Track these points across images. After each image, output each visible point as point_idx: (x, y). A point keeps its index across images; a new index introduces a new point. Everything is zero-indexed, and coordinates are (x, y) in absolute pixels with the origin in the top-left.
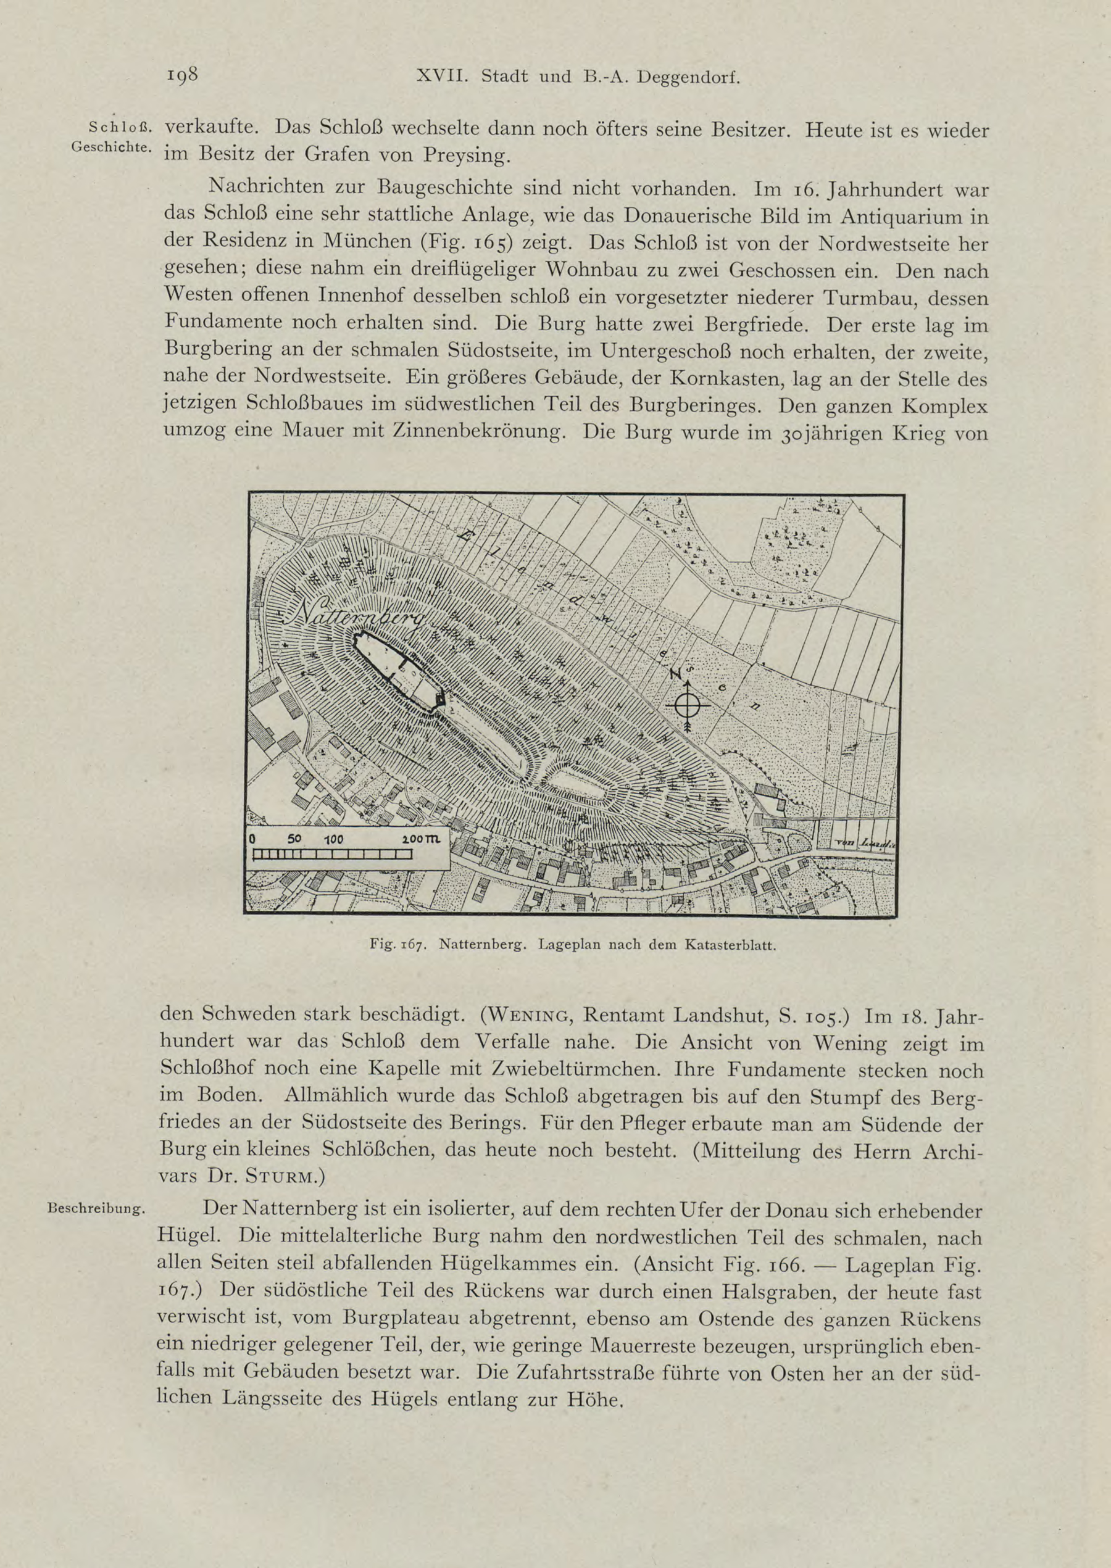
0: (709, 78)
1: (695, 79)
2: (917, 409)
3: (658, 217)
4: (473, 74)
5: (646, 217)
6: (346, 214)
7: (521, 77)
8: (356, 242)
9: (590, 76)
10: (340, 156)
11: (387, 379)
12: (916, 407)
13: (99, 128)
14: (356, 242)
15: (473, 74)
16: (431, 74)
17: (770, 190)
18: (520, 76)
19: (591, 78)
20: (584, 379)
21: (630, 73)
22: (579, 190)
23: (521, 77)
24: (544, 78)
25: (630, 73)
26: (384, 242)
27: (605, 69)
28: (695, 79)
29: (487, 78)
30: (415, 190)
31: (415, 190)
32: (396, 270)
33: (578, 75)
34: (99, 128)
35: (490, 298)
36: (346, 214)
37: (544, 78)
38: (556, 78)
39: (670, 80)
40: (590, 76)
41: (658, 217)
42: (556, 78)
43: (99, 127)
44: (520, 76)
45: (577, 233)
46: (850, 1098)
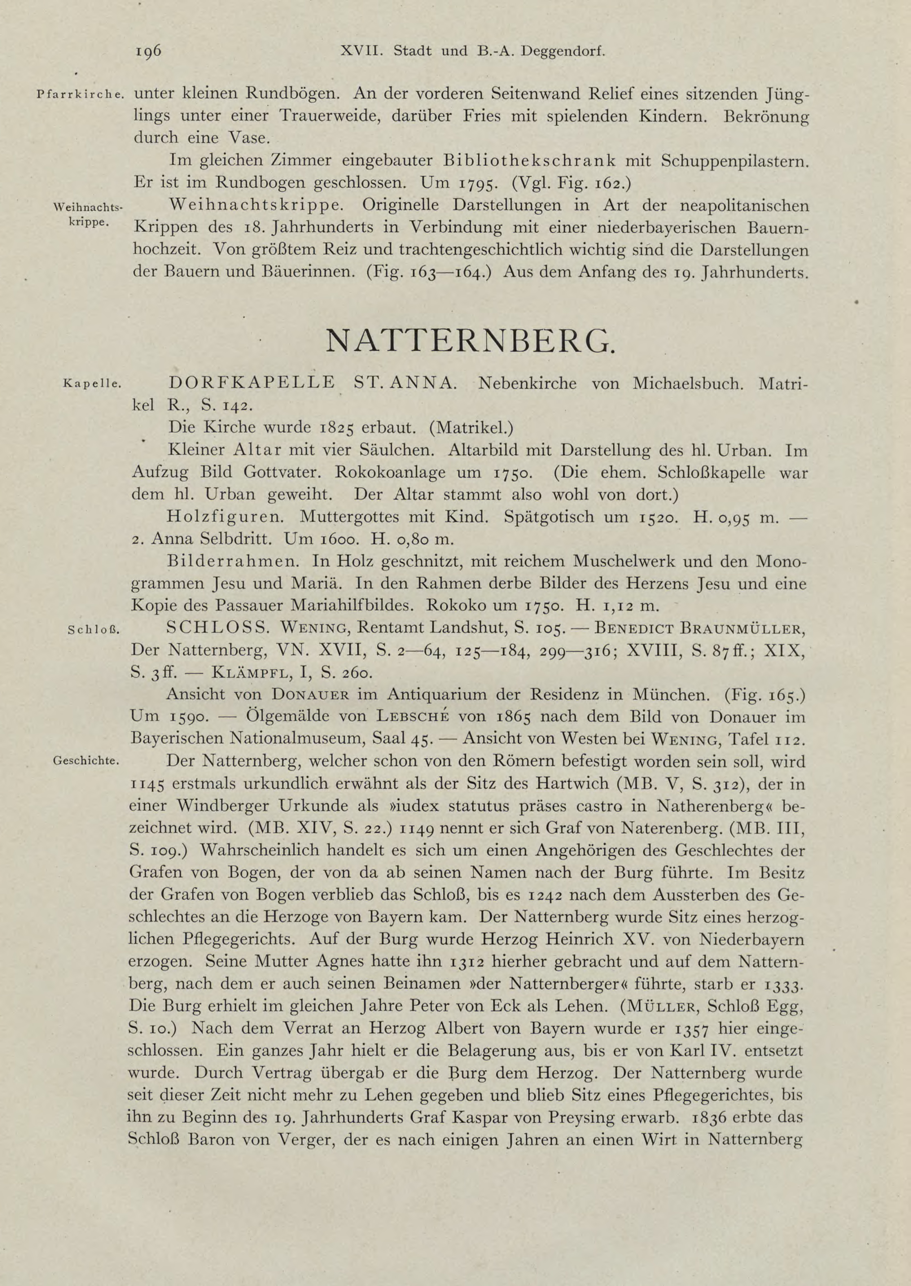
0: (579, 52)
1: (569, 52)
2: (144, 607)
3: (737, 718)
4: (387, 48)
5: (728, 719)
6: (321, 1095)
7: (426, 51)
8: (660, 695)
9: (483, 50)
10: (190, 896)
11: (176, 1075)
12: (143, 606)
13: (76, 631)
14: (660, 695)
15: (387, 48)
16: (352, 50)
17: (798, 452)
18: (426, 51)
19: (484, 52)
20: (283, 273)
21: (515, 48)
22: (602, 229)
23: (426, 51)
24: (445, 52)
25: (515, 48)
26: (620, 562)
27: (495, 46)
28: (569, 52)
29: (398, 53)
30: (179, 474)
31: (179, 474)
32: (585, 206)
33: (473, 50)
34: (76, 631)
35: (189, 1052)
36: (321, 1095)
37: (445, 52)
38: (455, 52)
39: (548, 53)
40: (483, 50)
41: (737, 718)
42: (455, 52)
43: (76, 629)
44: (426, 51)
45: (603, 1067)
46: (263, 562)
